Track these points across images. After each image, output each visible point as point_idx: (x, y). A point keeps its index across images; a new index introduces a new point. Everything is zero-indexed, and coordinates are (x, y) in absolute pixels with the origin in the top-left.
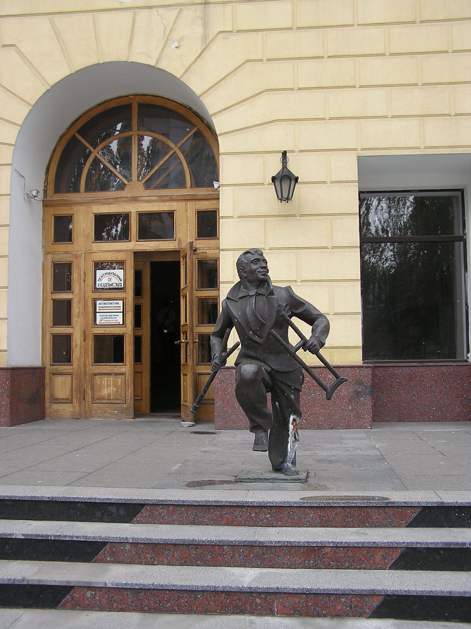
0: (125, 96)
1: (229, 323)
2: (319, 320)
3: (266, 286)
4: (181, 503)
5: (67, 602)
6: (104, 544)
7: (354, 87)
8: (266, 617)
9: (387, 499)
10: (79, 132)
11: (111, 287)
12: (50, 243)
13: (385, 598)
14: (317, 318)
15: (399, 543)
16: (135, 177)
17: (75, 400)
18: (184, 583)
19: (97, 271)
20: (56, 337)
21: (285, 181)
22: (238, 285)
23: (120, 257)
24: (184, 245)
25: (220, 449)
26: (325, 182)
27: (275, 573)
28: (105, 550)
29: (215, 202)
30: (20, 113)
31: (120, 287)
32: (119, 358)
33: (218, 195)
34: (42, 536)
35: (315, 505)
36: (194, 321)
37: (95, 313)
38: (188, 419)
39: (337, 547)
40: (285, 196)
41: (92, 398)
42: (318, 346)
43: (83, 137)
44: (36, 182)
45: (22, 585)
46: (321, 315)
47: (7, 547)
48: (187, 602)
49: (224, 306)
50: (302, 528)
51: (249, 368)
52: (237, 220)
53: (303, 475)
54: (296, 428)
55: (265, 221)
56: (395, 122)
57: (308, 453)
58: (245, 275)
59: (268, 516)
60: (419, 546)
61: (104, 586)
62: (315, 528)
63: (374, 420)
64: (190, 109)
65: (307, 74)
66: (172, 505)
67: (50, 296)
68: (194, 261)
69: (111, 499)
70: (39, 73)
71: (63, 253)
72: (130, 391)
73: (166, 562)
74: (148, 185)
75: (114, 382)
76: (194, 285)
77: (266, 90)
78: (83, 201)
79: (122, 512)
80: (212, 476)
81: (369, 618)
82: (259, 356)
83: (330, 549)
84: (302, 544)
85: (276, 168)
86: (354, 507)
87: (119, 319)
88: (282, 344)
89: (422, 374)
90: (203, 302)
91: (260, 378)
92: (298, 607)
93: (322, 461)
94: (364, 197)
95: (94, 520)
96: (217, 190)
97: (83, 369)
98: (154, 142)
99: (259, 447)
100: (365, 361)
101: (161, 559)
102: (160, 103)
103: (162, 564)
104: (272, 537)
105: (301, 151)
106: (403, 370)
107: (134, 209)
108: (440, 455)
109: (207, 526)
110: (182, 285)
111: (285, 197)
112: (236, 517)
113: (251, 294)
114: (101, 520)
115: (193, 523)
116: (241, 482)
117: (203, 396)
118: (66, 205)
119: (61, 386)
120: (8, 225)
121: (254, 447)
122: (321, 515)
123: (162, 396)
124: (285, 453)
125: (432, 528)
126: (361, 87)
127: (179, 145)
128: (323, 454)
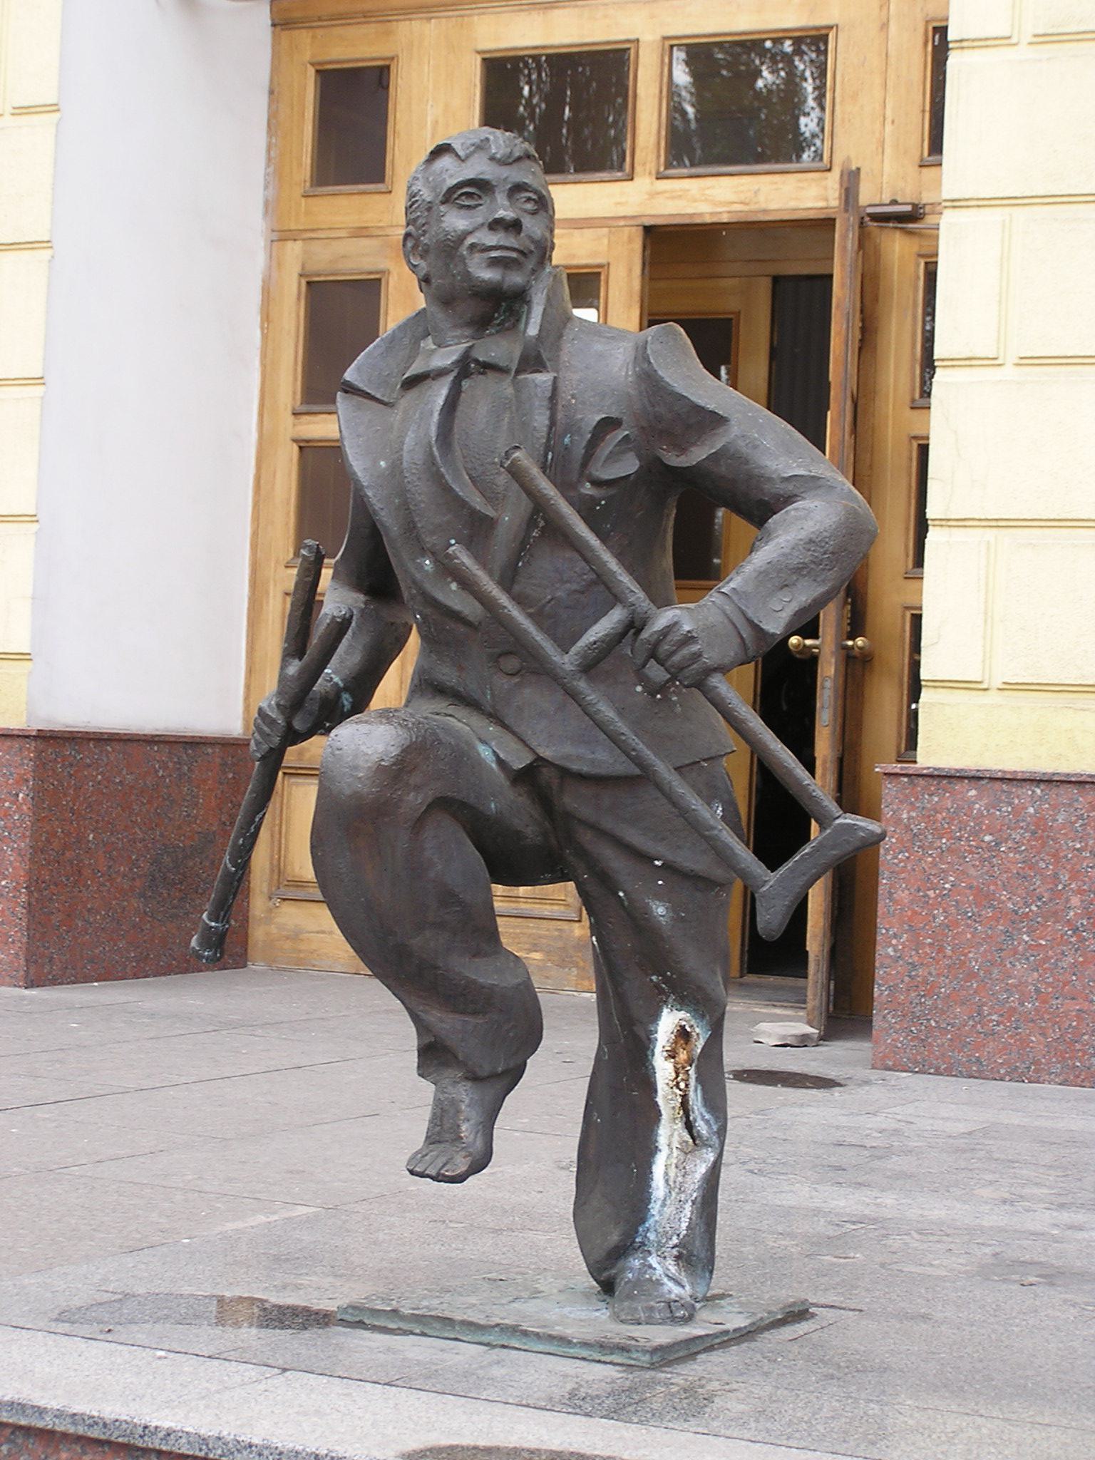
12: (298, 191)
67: (289, 428)
82: (472, 687)
116: (360, 1324)
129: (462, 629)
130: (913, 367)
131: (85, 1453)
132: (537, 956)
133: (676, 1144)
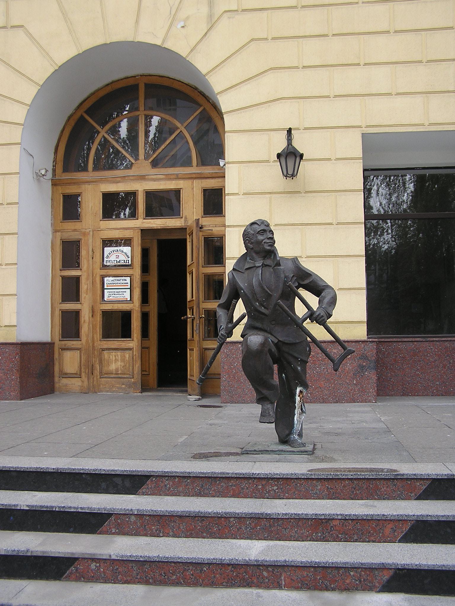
0: (132, 77)
1: (235, 294)
2: (326, 291)
3: (272, 257)
4: (187, 475)
5: (71, 573)
6: (109, 515)
7: (358, 64)
8: (273, 591)
9: (395, 471)
10: (87, 112)
11: (119, 264)
13: (396, 572)
14: (323, 290)
15: (409, 515)
16: (142, 155)
17: (83, 375)
18: (189, 556)
20: (65, 314)
21: (290, 157)
22: (244, 256)
23: (127, 234)
24: (191, 222)
25: (225, 422)
26: (329, 159)
27: (283, 546)
28: (110, 522)
29: (220, 180)
30: (28, 93)
32: (126, 333)
33: (224, 173)
34: (47, 507)
35: (323, 477)
36: (201, 297)
37: (103, 289)
38: (194, 393)
39: (346, 519)
40: (290, 172)
42: (325, 317)
44: (45, 161)
45: (26, 556)
46: (328, 286)
47: (12, 518)
48: (192, 575)
49: (230, 277)
50: (309, 500)
52: (243, 197)
53: (310, 448)
54: (304, 401)
55: (270, 198)
56: (399, 99)
57: (313, 426)
58: (251, 246)
59: (275, 488)
60: (429, 519)
61: (108, 558)
62: (322, 501)
63: (378, 395)
64: (196, 89)
65: (312, 52)
66: (178, 476)
67: (59, 273)
68: (200, 239)
69: (116, 471)
70: (48, 54)
71: (71, 229)
73: (171, 533)
74: (155, 164)
76: (200, 261)
77: (271, 69)
78: (92, 180)
79: (127, 484)
81: (379, 592)
83: (338, 521)
84: (310, 517)
85: (281, 145)
86: (363, 479)
87: (127, 295)
88: (289, 315)
89: (427, 349)
90: (209, 278)
91: (266, 349)
92: (307, 580)
93: (328, 433)
94: (368, 173)
95: (99, 491)
96: (223, 168)
97: (91, 345)
100: (370, 336)
101: (166, 531)
102: (166, 83)
103: (168, 536)
104: (279, 509)
105: (306, 129)
106: (407, 345)
107: (141, 187)
108: (447, 428)
109: (213, 498)
111: (290, 174)
112: (243, 489)
113: (257, 265)
114: (106, 491)
115: (199, 495)
116: (248, 454)
117: (209, 368)
118: (74, 183)
119: (70, 361)
120: (17, 203)
121: (260, 419)
123: (169, 370)
124: (291, 425)
125: (442, 501)
126: (365, 64)
127: (185, 124)
128: (329, 426)
129: (263, 316)
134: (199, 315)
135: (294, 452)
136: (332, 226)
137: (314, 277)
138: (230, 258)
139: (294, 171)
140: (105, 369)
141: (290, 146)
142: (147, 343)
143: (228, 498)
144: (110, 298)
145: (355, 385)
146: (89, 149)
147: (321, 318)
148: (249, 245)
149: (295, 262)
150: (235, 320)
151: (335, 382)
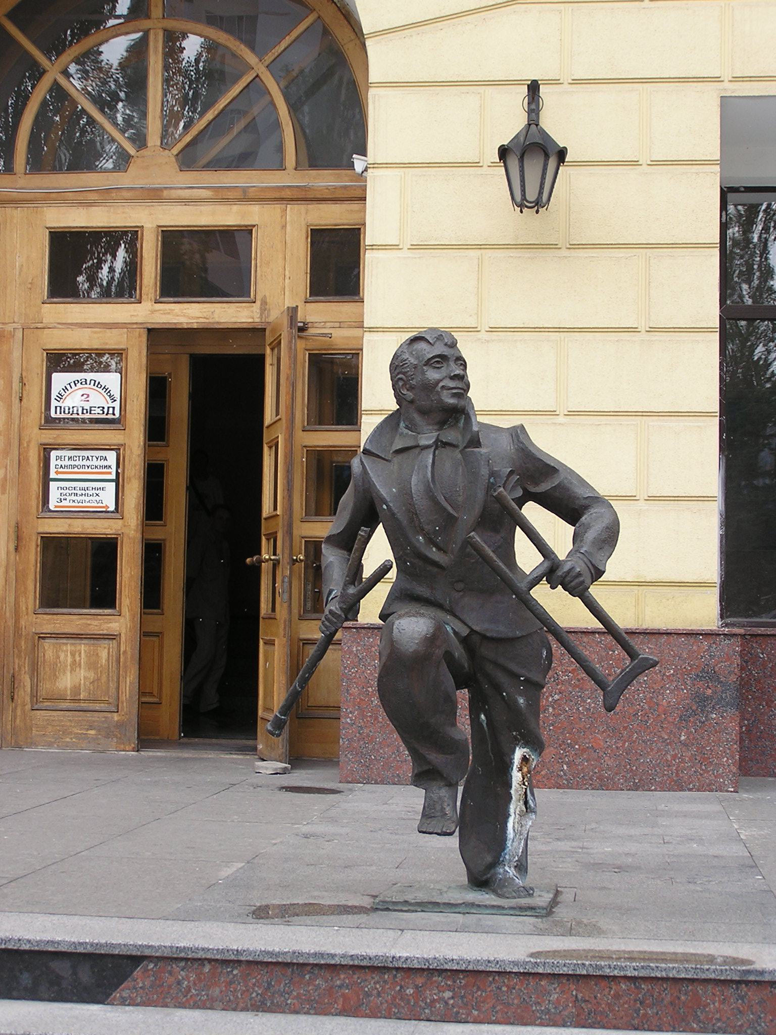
1: (368, 515)
2: (592, 511)
4: (233, 957)
9: (743, 962)
11: (88, 416)
14: (586, 508)
19: (55, 375)
21: (533, 156)
24: (276, 315)
26: (635, 163)
29: (355, 206)
31: (110, 416)
32: (104, 597)
35: (565, 970)
37: (46, 480)
40: (531, 196)
41: (32, 696)
43: (23, 30)
46: (597, 500)
50: (529, 1028)
51: (413, 627)
52: (410, 254)
53: (542, 899)
54: (530, 783)
58: (410, 395)
59: (448, 994)
66: (210, 961)
69: (59, 943)
72: (130, 680)
75: (88, 656)
78: (21, 196)
79: (85, 975)
80: (316, 893)
82: (439, 596)
85: (510, 124)
88: (496, 570)
91: (439, 652)
93: (597, 866)
96: (361, 176)
97: (11, 623)
98: (211, 47)
99: (434, 825)
100: (729, 621)
105: (576, 82)
107: (150, 219)
110: (269, 416)
112: (368, 995)
113: (423, 442)
114: (32, 994)
116: (387, 909)
122: (580, 996)
123: (212, 695)
124: (499, 841)
127: (269, 58)
128: (602, 849)
129: (436, 570)
130: (303, 409)
131: (354, 974)
132: (92, 732)
133: (517, 812)
134: (291, 555)
135: (503, 908)
136: (636, 337)
137: (562, 475)
138: (372, 412)
139: (541, 193)
140: (46, 687)
141: (533, 127)
142: (155, 622)
143: (331, 1017)
144: (64, 503)
145: (685, 744)
146: (23, 99)
147: (578, 580)
148: (405, 392)
149: (518, 436)
150: (367, 573)
151: (631, 736)
